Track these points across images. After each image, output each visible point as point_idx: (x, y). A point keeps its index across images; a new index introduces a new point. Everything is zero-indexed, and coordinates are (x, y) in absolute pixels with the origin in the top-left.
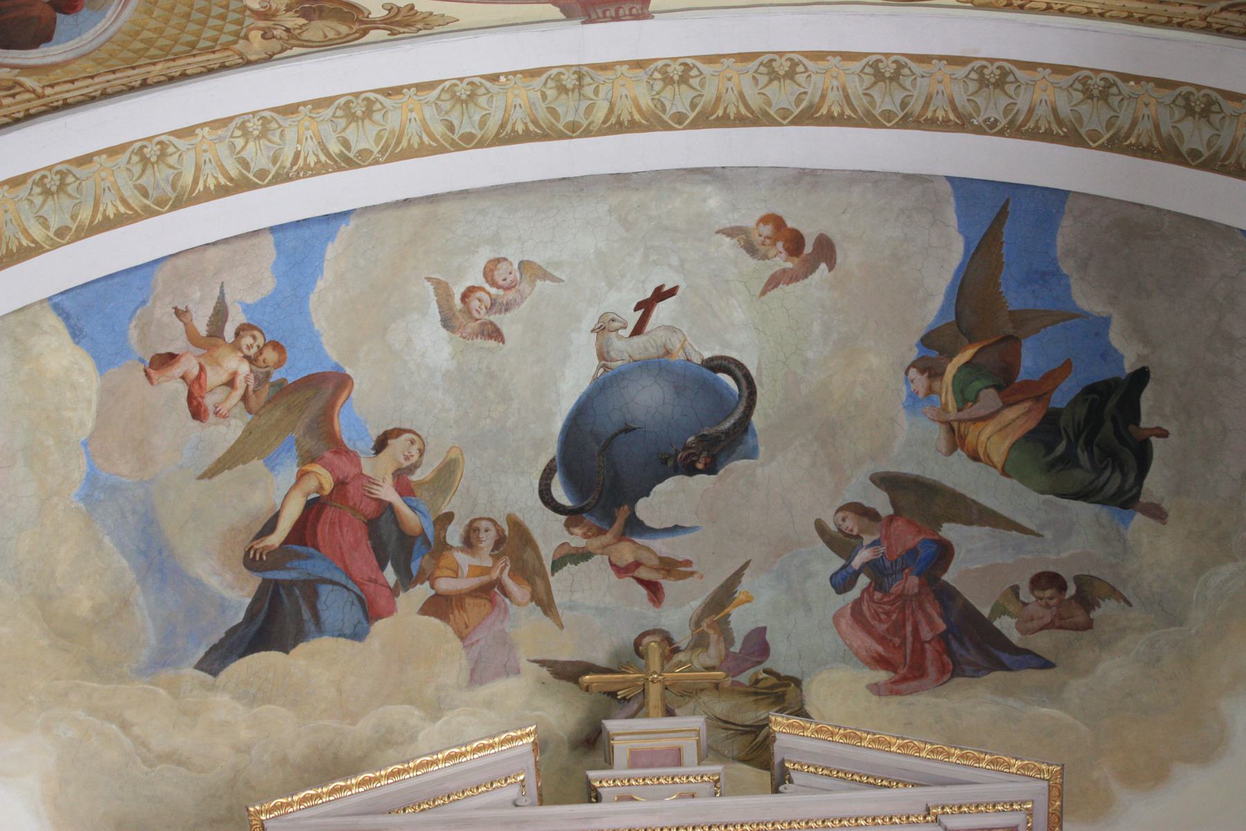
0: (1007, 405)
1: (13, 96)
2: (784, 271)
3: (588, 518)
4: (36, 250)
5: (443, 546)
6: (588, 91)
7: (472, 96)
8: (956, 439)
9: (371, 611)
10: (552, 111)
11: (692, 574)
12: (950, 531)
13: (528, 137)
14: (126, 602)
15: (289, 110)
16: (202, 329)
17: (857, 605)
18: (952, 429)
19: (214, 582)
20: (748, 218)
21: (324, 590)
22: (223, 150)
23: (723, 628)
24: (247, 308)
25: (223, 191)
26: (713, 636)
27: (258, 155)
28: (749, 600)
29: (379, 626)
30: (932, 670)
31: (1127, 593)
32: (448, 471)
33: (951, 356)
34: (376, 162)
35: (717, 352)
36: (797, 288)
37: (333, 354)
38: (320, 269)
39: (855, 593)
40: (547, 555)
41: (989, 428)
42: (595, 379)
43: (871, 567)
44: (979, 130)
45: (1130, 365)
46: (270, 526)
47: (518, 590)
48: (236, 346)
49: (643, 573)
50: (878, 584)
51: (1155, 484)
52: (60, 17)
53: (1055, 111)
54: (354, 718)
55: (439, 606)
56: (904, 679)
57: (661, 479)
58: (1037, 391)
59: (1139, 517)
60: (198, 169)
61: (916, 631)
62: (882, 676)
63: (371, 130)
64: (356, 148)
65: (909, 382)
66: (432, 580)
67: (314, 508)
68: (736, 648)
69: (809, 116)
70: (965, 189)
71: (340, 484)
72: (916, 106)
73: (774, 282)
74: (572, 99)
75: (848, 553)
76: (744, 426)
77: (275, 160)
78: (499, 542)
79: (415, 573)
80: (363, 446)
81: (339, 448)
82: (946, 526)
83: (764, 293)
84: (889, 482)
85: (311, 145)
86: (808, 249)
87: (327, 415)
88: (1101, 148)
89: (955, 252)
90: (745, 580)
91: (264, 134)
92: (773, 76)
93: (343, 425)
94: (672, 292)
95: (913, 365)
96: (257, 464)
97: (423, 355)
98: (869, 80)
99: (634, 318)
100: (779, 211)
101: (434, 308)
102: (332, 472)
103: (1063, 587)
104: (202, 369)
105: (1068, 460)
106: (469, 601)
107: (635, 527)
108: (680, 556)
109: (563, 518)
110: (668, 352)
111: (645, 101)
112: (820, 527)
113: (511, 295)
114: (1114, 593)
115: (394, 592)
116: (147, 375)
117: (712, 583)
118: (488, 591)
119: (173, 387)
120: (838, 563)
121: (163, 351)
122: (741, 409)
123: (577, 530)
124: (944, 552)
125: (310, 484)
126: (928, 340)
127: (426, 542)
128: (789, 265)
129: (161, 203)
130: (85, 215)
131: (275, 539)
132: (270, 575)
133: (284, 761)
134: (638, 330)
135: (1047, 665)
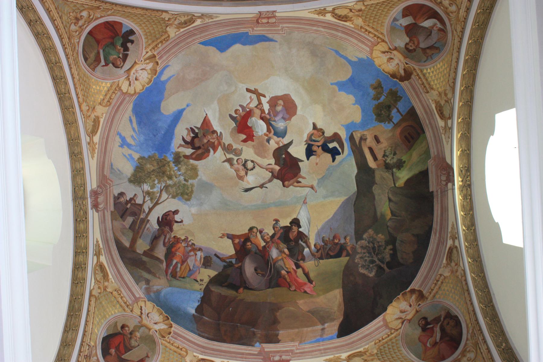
62: (354, 122)
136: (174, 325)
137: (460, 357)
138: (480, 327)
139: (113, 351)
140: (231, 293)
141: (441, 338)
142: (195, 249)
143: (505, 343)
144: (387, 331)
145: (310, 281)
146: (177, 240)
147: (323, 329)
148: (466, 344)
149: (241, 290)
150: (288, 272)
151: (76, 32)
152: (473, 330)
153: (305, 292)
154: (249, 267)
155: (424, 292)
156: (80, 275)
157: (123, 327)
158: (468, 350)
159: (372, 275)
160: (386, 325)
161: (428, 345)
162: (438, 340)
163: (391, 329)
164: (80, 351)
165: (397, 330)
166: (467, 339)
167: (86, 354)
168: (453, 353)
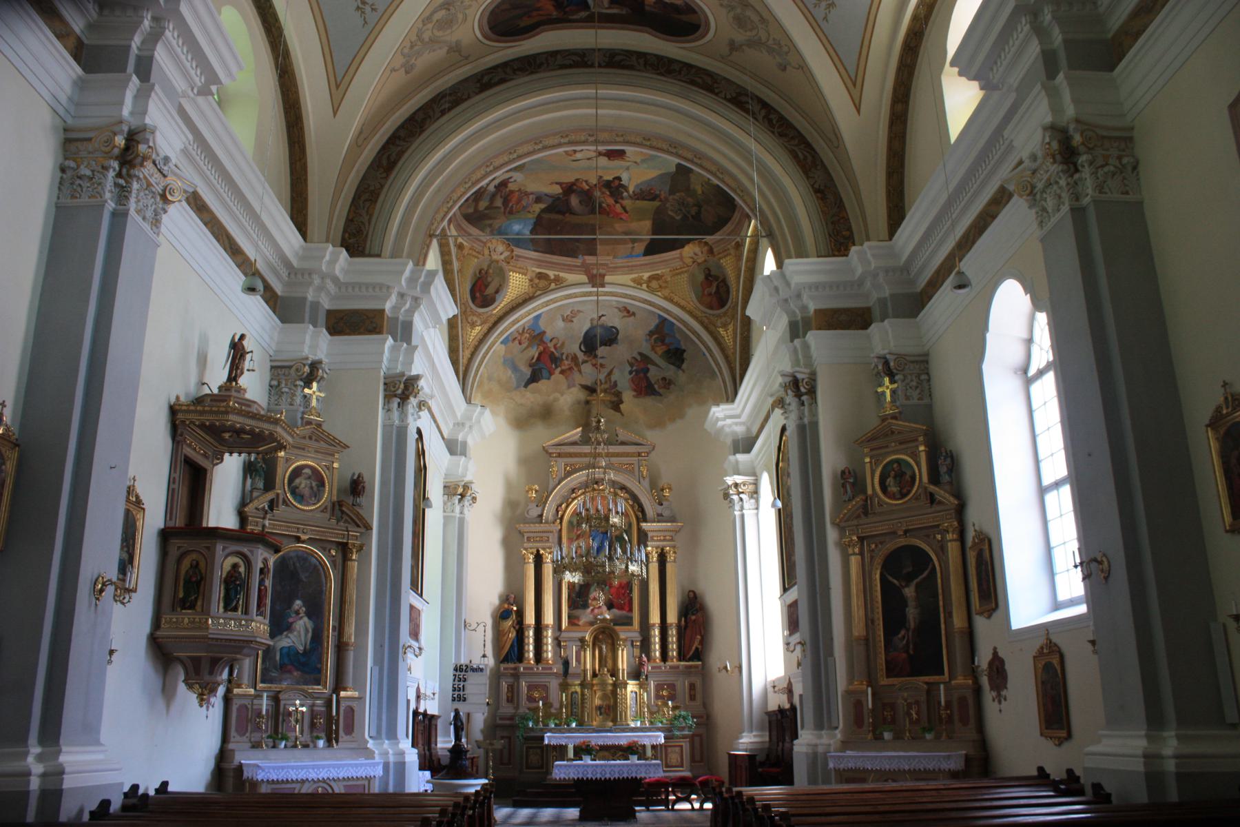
5: (562, 359)
8: (653, 349)
9: (551, 373)
12: (649, 366)
32: (563, 344)
37: (543, 329)
43: (636, 371)
47: (575, 369)
50: (636, 375)
51: (684, 366)
55: (562, 372)
62: (634, 393)
70: (660, 316)
71: (544, 349)
75: (632, 367)
76: (616, 338)
78: (572, 358)
80: (548, 341)
81: (544, 343)
84: (640, 354)
87: (542, 338)
93: (545, 339)
108: (604, 363)
114: (674, 384)
117: (609, 370)
118: (570, 369)
119: (517, 342)
120: (630, 369)
124: (648, 370)
126: (650, 332)
131: (534, 361)
135: (661, 395)
136: (515, 249)
139: (478, 295)
140: (560, 217)
141: (715, 293)
142: (527, 194)
144: (681, 263)
145: (626, 212)
146: (512, 192)
147: (633, 247)
149: (567, 215)
150: (608, 205)
153: (621, 219)
154: (574, 201)
155: (715, 250)
156: (448, 267)
157: (480, 272)
159: (678, 218)
160: (681, 258)
161: (706, 292)
163: (684, 263)
165: (688, 266)
168: (718, 309)
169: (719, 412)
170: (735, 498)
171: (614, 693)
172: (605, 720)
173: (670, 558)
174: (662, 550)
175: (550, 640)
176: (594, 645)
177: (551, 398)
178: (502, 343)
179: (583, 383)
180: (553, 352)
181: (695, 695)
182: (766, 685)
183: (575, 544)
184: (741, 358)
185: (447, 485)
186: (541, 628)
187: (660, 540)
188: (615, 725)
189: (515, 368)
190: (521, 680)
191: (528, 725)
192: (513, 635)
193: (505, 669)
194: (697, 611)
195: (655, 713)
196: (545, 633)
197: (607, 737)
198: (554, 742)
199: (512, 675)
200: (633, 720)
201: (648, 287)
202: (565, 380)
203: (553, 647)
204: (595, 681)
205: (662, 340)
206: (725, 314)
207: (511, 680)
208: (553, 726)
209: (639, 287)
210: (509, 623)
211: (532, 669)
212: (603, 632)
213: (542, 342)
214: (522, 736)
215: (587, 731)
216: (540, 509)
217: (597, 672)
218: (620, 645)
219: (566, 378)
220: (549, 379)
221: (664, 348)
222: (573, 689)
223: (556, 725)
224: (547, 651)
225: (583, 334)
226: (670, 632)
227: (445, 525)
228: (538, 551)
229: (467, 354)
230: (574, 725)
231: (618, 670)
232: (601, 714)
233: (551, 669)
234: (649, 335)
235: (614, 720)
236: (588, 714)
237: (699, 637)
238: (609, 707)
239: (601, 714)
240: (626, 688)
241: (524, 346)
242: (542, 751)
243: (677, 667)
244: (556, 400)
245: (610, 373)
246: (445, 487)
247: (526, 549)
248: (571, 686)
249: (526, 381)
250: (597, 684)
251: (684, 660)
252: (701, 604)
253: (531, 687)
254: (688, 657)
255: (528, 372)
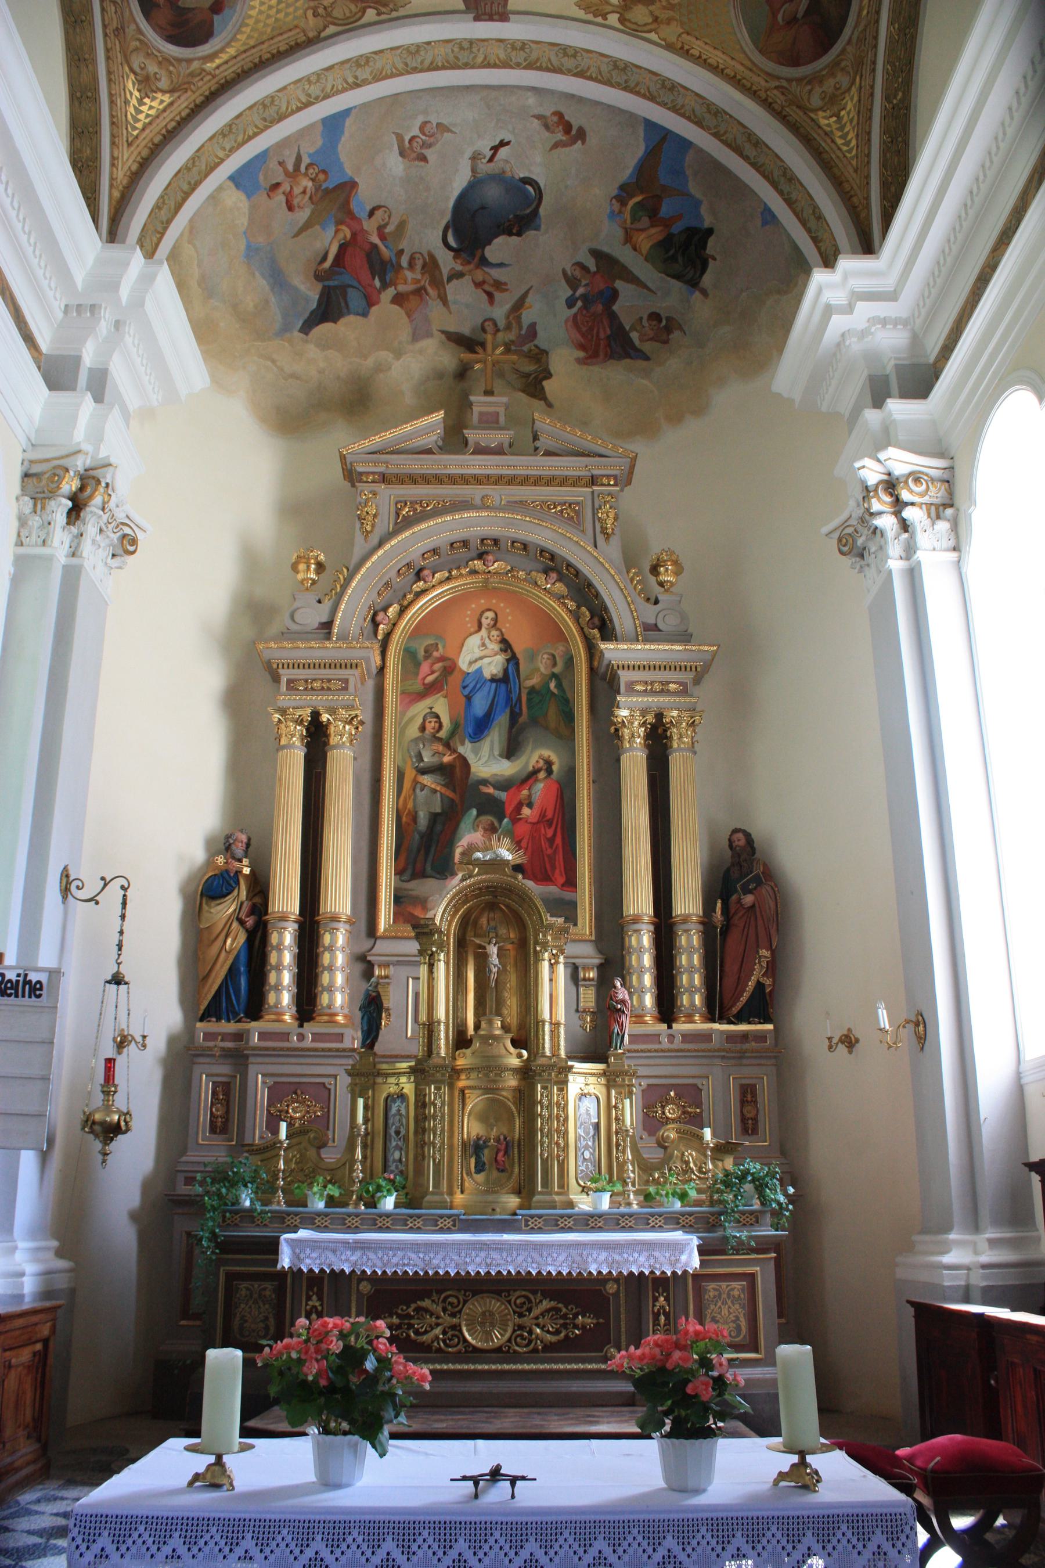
0: (652, 226)
1: (202, 79)
2: (561, 141)
3: (464, 255)
4: (222, 161)
6: (475, 50)
7: (418, 51)
8: (628, 239)
9: (371, 302)
10: (457, 58)
11: (507, 290)
12: (619, 284)
13: (443, 68)
14: (267, 301)
15: (331, 68)
16: (290, 168)
17: (575, 316)
18: (626, 233)
19: (302, 288)
20: (547, 110)
21: (349, 290)
22: (299, 92)
23: (518, 319)
24: (310, 155)
25: (299, 109)
26: (514, 325)
27: (314, 90)
28: (530, 307)
29: (374, 309)
30: (602, 354)
31: (686, 328)
32: (402, 225)
33: (632, 197)
34: (370, 83)
35: (527, 175)
36: (567, 150)
38: (343, 132)
39: (575, 310)
40: (445, 272)
41: (642, 236)
42: (469, 182)
43: (584, 297)
44: (658, 104)
45: (707, 224)
46: (324, 258)
48: (306, 174)
49: (487, 287)
50: (585, 307)
51: (707, 280)
52: (216, 17)
53: (694, 111)
54: (365, 357)
55: (399, 299)
56: (590, 357)
57: (496, 237)
58: (667, 223)
59: (697, 294)
60: (288, 103)
61: (598, 333)
62: (581, 354)
63: (368, 70)
64: (360, 78)
65: (612, 205)
66: (395, 285)
67: (343, 248)
68: (523, 332)
69: (581, 74)
70: (650, 126)
71: (354, 235)
72: (632, 84)
73: (556, 145)
74: (466, 53)
75: (575, 290)
76: (535, 213)
77: (323, 91)
78: (424, 267)
79: (388, 281)
80: (363, 215)
82: (617, 281)
83: (551, 149)
84: (596, 254)
85: (340, 81)
86: (574, 132)
87: (347, 202)
88: (711, 134)
89: (640, 151)
90: (530, 295)
91: (318, 81)
92: (565, 54)
93: (354, 206)
94: (508, 143)
95: (615, 197)
96: (317, 227)
97: (390, 170)
98: (611, 67)
99: (489, 154)
100: (563, 110)
101: (396, 147)
102: (350, 229)
103: (660, 321)
104: (291, 188)
105: (673, 259)
106: (411, 297)
107: (484, 262)
108: (503, 279)
109: (452, 254)
110: (504, 172)
111: (502, 56)
112: (564, 272)
113: (432, 140)
115: (379, 292)
116: (268, 195)
117: (517, 295)
118: (420, 292)
119: (280, 198)
120: (570, 293)
121: (274, 182)
122: (534, 206)
123: (459, 261)
124: (614, 295)
125: (341, 235)
126: (622, 188)
127: (392, 265)
128: (564, 138)
129: (271, 122)
130: (240, 139)
131: (327, 264)
132: (327, 283)
133: (338, 378)
134: (491, 160)
135: (647, 358)
137: (824, 73)
138: (877, 32)
143: (904, 93)
148: (843, 51)
151: (171, 72)
152: (866, 26)
158: (843, 64)
161: (780, 18)
162: (800, 15)
164: (105, 26)
166: (849, 42)
167: (115, 25)
169: (832, 286)
170: (887, 522)
171: (525, 1098)
172: (492, 1188)
173: (679, 740)
174: (659, 716)
175: (340, 959)
176: (461, 944)
177: (370, 362)
178: (237, 179)
179: (452, 329)
180: (375, 246)
181: (755, 1120)
182: (1018, 1076)
183: (420, 708)
184: (884, 164)
185: (36, 469)
186: (318, 923)
187: (653, 692)
188: (526, 1205)
189: (277, 279)
190: (252, 1069)
191: (237, 1201)
192: (236, 941)
193: (208, 1036)
194: (758, 881)
195: (659, 1167)
196: (327, 939)
197: (499, 1247)
198: (311, 1263)
199: (228, 1055)
200: (585, 1190)
201: (622, 20)
202: (406, 319)
203: (348, 980)
204: (464, 1060)
205: (650, 210)
206: (835, 66)
207: (224, 1069)
208: (321, 1205)
209: (599, 20)
210: (226, 909)
211: (285, 1036)
212: (492, 906)
213: (346, 215)
214: (214, 1236)
215: (434, 1224)
216: (327, 604)
217: (471, 1031)
218: (545, 946)
219: (409, 316)
220: (365, 314)
221: (656, 233)
222: (391, 1087)
223: (331, 1202)
224: (330, 989)
225: (451, 203)
226: (683, 940)
227: (17, 582)
228: (315, 715)
229: (129, 159)
230: (389, 1203)
231: (539, 1023)
232: (480, 1168)
233: (340, 1037)
234: (618, 198)
235: (525, 1190)
236: (437, 1167)
237: (764, 952)
238: (506, 1146)
239: (480, 1168)
240: (563, 1084)
241: (303, 215)
242: (281, 1291)
243: (706, 1037)
244: (380, 368)
245: (519, 305)
246: (26, 475)
247: (283, 712)
248: (387, 1075)
249: (307, 315)
250: (470, 1070)
251: (722, 1018)
252: (765, 865)
253: (279, 1092)
254: (735, 1010)
255: (311, 293)
